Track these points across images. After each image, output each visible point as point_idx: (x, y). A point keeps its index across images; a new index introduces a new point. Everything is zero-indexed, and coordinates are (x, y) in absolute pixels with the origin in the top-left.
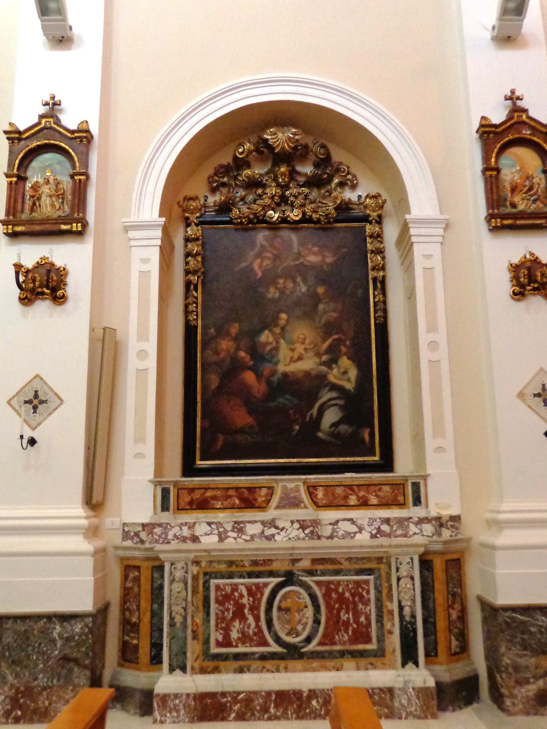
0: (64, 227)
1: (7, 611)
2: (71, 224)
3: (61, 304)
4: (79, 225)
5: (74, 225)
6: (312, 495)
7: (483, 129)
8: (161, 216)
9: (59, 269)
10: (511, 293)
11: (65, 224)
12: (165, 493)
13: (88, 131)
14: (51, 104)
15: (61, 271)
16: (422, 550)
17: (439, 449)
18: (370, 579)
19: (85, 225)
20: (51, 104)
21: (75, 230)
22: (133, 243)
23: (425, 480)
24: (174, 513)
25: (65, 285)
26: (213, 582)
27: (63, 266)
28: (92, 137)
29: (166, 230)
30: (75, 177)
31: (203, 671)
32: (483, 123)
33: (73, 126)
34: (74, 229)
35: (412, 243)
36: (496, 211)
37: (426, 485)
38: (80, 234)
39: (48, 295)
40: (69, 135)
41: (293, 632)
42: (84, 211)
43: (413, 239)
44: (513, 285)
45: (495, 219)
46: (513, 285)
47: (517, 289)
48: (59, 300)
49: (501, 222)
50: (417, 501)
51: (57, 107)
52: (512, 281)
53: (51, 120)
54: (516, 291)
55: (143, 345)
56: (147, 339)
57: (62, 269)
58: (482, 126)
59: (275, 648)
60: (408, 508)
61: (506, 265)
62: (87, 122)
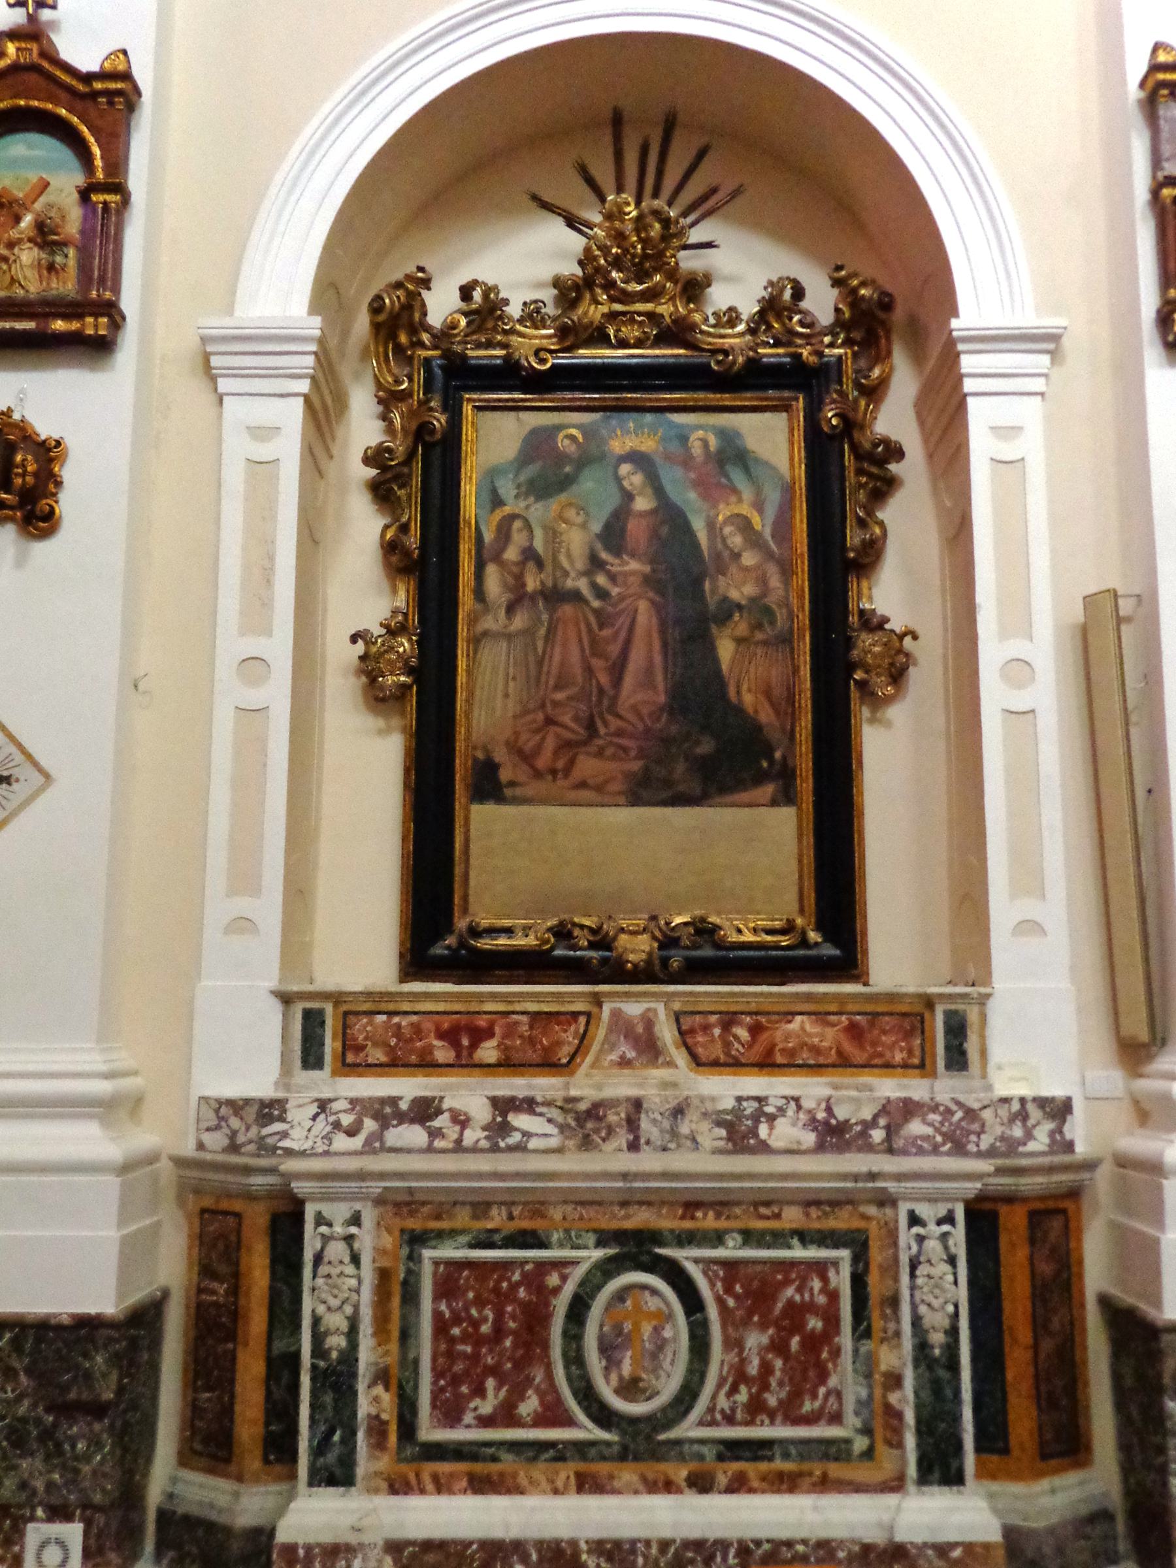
0: (59, 325)
1: (731, 1078)
2: (80, 316)
4: (104, 320)
5: (90, 320)
6: (685, 1036)
7: (1161, 76)
8: (314, 309)
9: (44, 442)
11: (65, 317)
12: (313, 1021)
17: (1030, 927)
18: (842, 1258)
19: (117, 321)
21: (92, 332)
24: (335, 1073)
25: (59, 484)
26: (845, 1254)
27: (56, 436)
28: (139, 93)
29: (326, 361)
30: (94, 198)
31: (398, 1486)
32: (1162, 58)
34: (90, 331)
35: (965, 395)
39: (11, 508)
40: (81, 87)
41: (631, 1388)
42: (116, 290)
43: (969, 385)
53: (34, 47)
57: (53, 443)
58: (1155, 68)
59: (587, 1430)
60: (933, 1074)
62: (125, 52)
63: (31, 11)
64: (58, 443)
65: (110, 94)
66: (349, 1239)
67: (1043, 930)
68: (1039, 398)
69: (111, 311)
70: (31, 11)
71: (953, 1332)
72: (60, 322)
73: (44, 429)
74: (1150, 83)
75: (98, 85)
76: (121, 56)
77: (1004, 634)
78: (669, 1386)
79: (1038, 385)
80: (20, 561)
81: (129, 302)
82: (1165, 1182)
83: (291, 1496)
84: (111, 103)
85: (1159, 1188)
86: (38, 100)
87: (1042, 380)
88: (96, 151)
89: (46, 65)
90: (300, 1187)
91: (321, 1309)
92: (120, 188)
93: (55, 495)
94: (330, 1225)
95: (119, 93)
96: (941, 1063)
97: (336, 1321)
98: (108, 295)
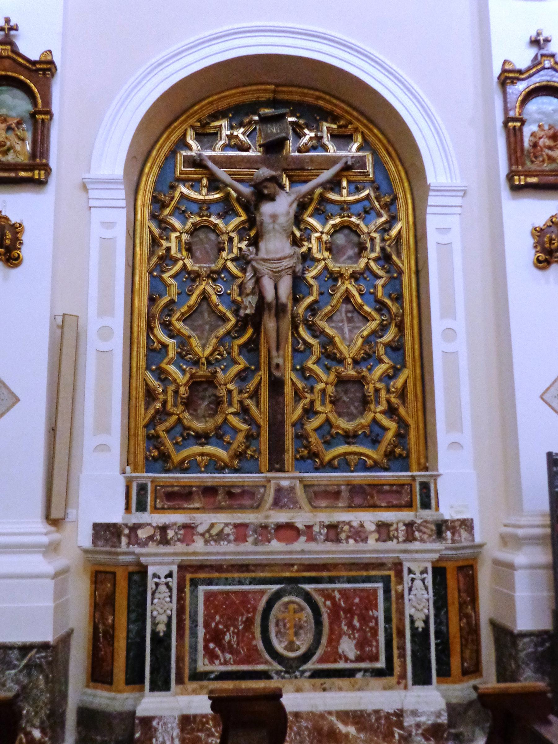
0: (22, 174)
3: (16, 266)
4: (43, 172)
9: (14, 224)
10: (535, 261)
13: (52, 62)
14: (6, 29)
15: (17, 228)
16: (436, 556)
17: (455, 445)
20: (6, 29)
22: (92, 203)
23: (435, 480)
25: (21, 244)
27: (19, 222)
32: (507, 67)
33: (34, 56)
36: (520, 168)
37: (436, 484)
38: (41, 183)
42: (47, 158)
44: (537, 252)
45: (519, 176)
46: (537, 252)
47: (542, 256)
48: (14, 262)
49: (525, 179)
50: (426, 505)
51: (13, 32)
52: (535, 247)
53: (9, 47)
54: (540, 258)
55: (107, 321)
56: (112, 315)
58: (504, 71)
61: (530, 228)
62: (50, 51)
63: (6, 32)
64: (20, 225)
65: (44, 70)
66: (167, 584)
67: (462, 447)
68: (458, 215)
69: (47, 168)
70: (6, 32)
71: (169, 625)
72: (23, 173)
73: (14, 219)
74: (503, 77)
75: (38, 66)
76: (49, 53)
77: (443, 316)
78: (303, 646)
79: (458, 210)
80: (6, 278)
81: (53, 163)
82: (515, 572)
83: (143, 696)
84: (44, 74)
85: (513, 576)
86: (11, 72)
87: (459, 208)
88: (38, 96)
89: (14, 56)
90: (143, 560)
91: (155, 613)
92: (49, 113)
93: (20, 249)
94: (159, 578)
95: (49, 70)
96: (419, 505)
97: (163, 618)
98: (44, 161)
